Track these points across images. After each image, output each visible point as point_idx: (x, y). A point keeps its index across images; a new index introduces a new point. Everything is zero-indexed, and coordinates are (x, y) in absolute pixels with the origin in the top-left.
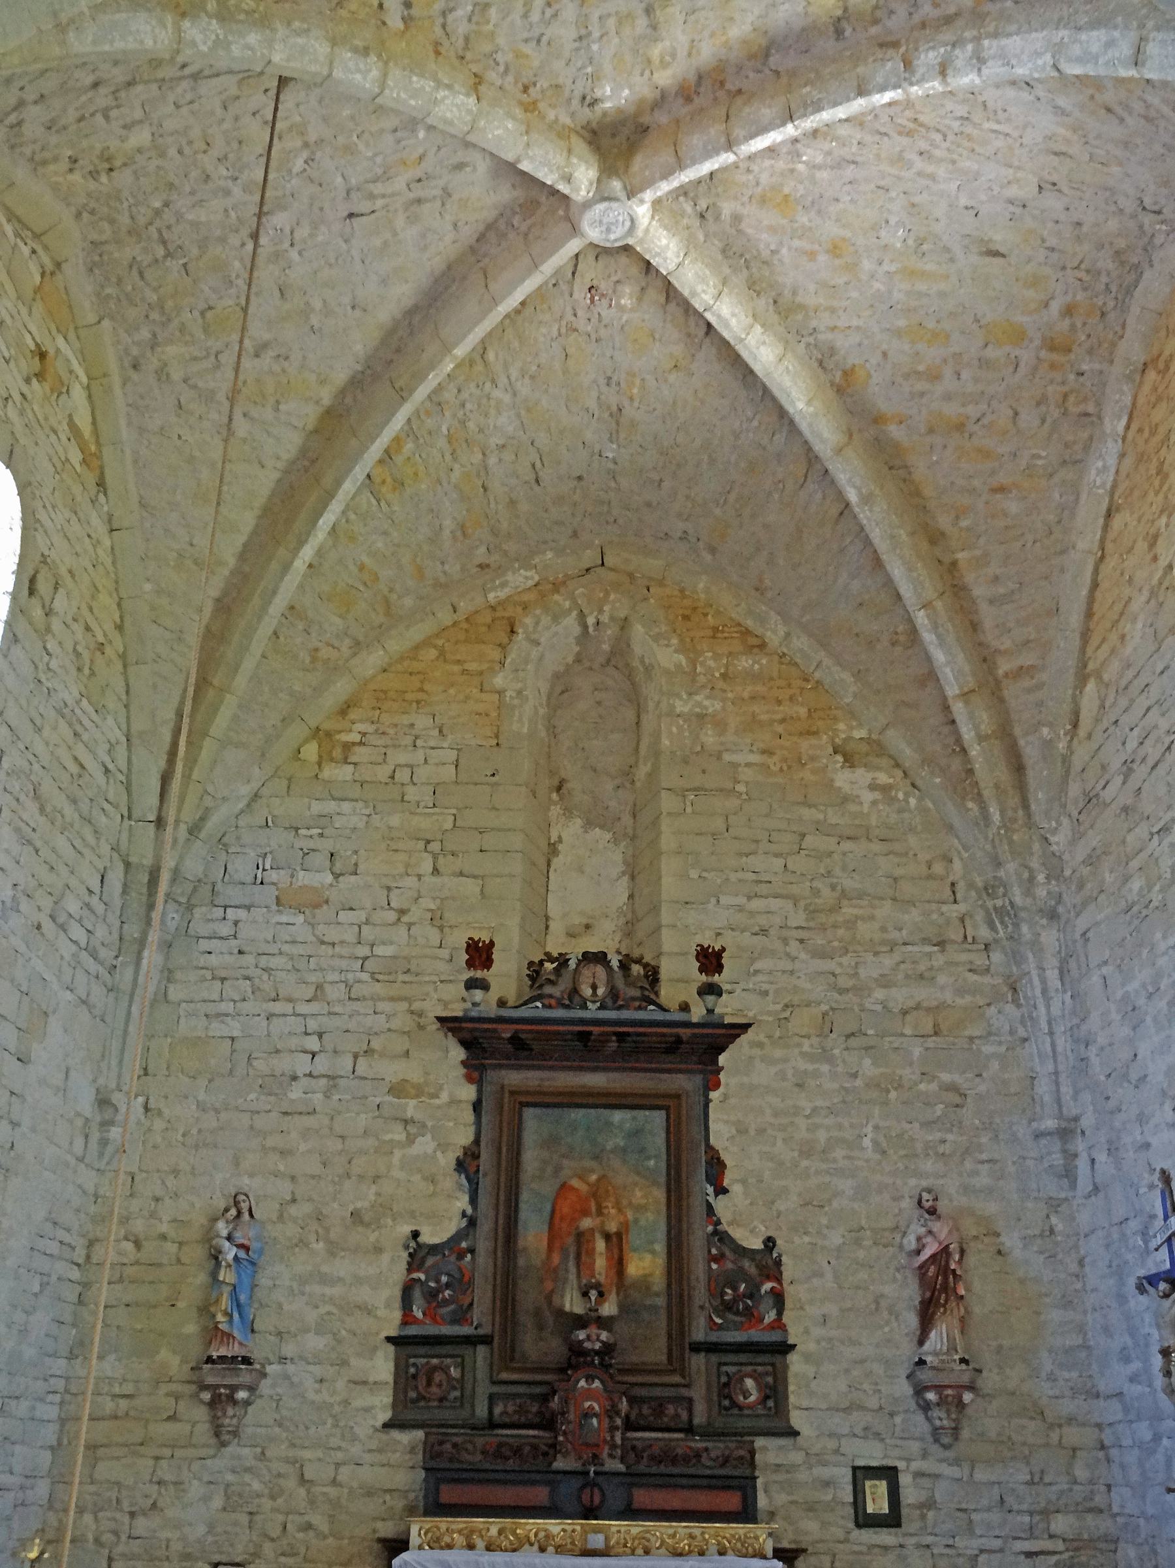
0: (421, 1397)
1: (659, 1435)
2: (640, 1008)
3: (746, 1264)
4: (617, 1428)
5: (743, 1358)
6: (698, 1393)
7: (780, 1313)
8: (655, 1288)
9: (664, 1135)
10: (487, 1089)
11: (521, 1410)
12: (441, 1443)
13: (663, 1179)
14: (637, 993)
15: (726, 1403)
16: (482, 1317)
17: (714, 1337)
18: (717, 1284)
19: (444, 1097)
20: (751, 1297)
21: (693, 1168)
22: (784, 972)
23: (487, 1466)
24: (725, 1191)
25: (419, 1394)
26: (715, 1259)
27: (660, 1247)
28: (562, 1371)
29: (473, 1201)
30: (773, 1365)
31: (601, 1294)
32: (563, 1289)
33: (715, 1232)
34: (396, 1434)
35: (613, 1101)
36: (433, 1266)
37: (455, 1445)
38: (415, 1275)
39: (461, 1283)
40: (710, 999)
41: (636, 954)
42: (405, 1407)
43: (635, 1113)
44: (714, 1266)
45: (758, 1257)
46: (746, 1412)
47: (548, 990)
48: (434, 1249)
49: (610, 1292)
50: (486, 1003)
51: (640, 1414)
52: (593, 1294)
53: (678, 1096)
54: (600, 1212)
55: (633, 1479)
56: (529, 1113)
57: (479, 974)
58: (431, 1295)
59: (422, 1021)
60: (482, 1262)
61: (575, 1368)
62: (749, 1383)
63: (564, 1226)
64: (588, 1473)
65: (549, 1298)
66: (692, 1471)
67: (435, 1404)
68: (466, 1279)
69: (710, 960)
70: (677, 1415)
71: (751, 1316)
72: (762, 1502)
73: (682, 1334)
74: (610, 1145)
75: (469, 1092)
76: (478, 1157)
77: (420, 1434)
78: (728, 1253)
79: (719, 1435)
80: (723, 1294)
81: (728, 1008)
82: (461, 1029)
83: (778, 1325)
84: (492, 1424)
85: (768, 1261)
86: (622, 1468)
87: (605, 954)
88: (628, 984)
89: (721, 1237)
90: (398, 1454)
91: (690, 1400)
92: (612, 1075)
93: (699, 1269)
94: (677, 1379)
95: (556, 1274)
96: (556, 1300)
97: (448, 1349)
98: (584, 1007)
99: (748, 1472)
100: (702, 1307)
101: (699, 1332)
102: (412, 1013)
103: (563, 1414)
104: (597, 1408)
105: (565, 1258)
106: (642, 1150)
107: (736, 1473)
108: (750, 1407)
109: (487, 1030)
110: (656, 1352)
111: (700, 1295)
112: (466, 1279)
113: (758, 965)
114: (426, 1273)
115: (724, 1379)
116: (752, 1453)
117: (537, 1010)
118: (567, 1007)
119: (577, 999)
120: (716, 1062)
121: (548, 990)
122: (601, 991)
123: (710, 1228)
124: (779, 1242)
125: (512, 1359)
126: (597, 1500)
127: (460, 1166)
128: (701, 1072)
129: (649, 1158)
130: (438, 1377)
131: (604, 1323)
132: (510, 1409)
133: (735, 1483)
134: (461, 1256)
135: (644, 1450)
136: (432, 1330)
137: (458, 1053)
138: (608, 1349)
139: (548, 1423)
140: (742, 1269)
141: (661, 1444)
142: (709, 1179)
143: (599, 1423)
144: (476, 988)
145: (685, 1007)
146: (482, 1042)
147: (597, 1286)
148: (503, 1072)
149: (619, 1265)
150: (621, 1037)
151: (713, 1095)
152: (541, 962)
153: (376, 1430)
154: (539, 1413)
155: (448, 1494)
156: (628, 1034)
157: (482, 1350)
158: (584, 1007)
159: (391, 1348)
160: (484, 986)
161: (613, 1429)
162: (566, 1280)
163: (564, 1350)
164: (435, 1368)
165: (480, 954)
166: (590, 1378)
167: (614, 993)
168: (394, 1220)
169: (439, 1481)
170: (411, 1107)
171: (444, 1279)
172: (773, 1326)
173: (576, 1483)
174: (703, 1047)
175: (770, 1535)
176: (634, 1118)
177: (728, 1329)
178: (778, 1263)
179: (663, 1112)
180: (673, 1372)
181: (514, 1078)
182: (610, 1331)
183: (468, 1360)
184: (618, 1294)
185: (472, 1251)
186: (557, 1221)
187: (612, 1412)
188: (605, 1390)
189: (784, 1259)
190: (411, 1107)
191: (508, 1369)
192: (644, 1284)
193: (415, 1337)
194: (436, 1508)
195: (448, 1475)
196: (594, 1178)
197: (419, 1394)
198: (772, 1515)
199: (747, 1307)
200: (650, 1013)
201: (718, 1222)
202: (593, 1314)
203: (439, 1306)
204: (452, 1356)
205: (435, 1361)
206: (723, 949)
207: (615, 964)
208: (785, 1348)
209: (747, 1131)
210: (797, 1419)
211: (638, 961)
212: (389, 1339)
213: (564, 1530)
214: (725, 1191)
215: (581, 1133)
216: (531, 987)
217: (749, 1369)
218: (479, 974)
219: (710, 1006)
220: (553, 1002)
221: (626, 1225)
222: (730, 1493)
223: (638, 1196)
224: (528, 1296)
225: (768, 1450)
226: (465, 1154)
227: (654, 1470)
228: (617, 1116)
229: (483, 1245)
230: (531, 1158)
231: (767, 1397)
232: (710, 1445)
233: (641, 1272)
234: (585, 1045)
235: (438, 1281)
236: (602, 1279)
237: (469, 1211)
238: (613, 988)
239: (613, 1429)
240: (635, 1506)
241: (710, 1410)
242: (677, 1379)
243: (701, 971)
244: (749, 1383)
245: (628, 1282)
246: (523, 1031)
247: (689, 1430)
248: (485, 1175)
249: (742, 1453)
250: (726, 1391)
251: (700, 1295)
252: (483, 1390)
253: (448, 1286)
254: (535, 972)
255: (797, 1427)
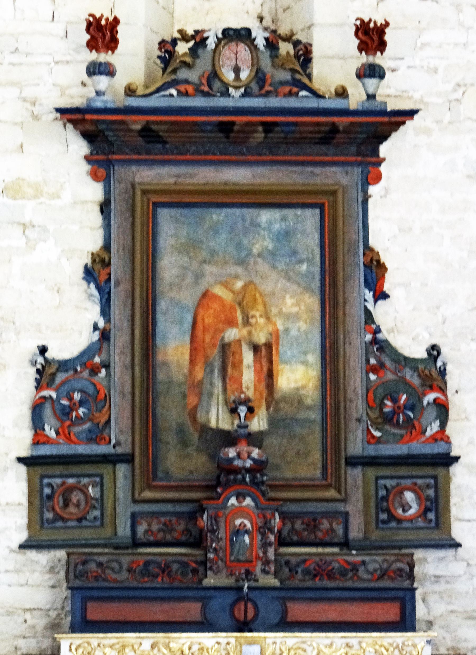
0: (58, 518)
1: (313, 550)
2: (290, 94)
3: (409, 374)
4: (270, 544)
5: (403, 471)
6: (355, 507)
7: (443, 425)
8: (309, 401)
9: (317, 236)
10: (116, 189)
11: (168, 528)
12: (84, 563)
13: (316, 284)
14: (286, 76)
15: (384, 516)
16: (120, 434)
17: (371, 451)
18: (374, 399)
19: (67, 197)
20: (412, 408)
21: (348, 272)
22: (456, 45)
23: (135, 584)
24: (385, 296)
25: (56, 514)
26: (374, 369)
27: (314, 358)
28: (210, 488)
29: (105, 311)
30: (435, 478)
31: (251, 410)
32: (209, 405)
33: (375, 341)
34: (32, 554)
35: (260, 199)
36: (63, 383)
37: (100, 564)
38: (45, 393)
39: (97, 400)
40: (371, 83)
41: (283, 30)
42: (42, 526)
43: (289, 212)
44: (373, 377)
45: (421, 366)
46: (405, 525)
47: (183, 74)
48: (64, 365)
49: (260, 407)
50: (111, 91)
51: (293, 529)
52: (243, 410)
53: (334, 193)
54: (247, 322)
55: (287, 593)
56: (164, 215)
57: (103, 57)
58: (64, 414)
59: (36, 110)
60: (119, 378)
61: (226, 486)
62: (409, 496)
63: (208, 338)
64: (241, 588)
65: (193, 415)
66: (349, 584)
67: (74, 523)
68: (102, 395)
69: (371, 37)
70: (332, 530)
71: (412, 428)
72: (421, 611)
73: (337, 450)
74: (256, 249)
75: (95, 192)
76: (109, 264)
77: (61, 554)
78: (388, 363)
79: (377, 548)
80: (382, 405)
81: (391, 93)
82: (83, 121)
83: (442, 436)
84: (136, 543)
85: (431, 370)
86: (275, 582)
87: (248, 31)
88: (274, 66)
89: (381, 346)
90: (37, 575)
91: (346, 514)
92: (260, 170)
93: (356, 380)
94: (332, 493)
95: (198, 388)
96: (201, 417)
97: (87, 469)
98: (226, 94)
99: (406, 584)
100: (359, 420)
101: (356, 445)
102: (24, 100)
103: (213, 531)
104: (249, 525)
105: (209, 367)
106: (294, 253)
107: (393, 585)
108: (410, 520)
109: (113, 122)
110: (309, 467)
111: (357, 406)
112: (102, 395)
113: (425, 38)
114: (57, 390)
115: (382, 493)
116: (412, 566)
117: (172, 98)
118: (206, 94)
119: (217, 85)
120: (376, 152)
121: (183, 74)
122: (244, 75)
123: (369, 337)
124: (444, 350)
125: (155, 477)
126: (251, 614)
127: (89, 274)
128: (359, 164)
129: (301, 262)
130: (76, 497)
131: (255, 439)
132: (155, 527)
133: (393, 594)
134: (94, 371)
135: (298, 565)
136: (65, 449)
137: (79, 147)
138: (259, 466)
139: (197, 541)
140: (403, 379)
141: (317, 559)
142: (367, 285)
143: (251, 540)
144: (101, 73)
145: (342, 93)
146: (104, 133)
147: (246, 401)
148: (134, 168)
149: (269, 377)
150: (268, 127)
151: (372, 190)
152: (174, 42)
153: (12, 551)
154: (187, 530)
155: (95, 612)
156: (275, 124)
157: (122, 470)
158: (226, 94)
159: (23, 469)
160: (108, 70)
161: (266, 545)
162: (211, 395)
163: (212, 468)
164: (71, 489)
165: (103, 34)
166: (240, 496)
167: (259, 77)
168: (18, 333)
169: (85, 601)
170: (29, 210)
171: (77, 396)
172: (434, 439)
173: (230, 597)
174: (362, 135)
175: (429, 642)
176: (284, 219)
177: (386, 442)
178: (443, 373)
179: (317, 211)
180: (328, 486)
181: (147, 175)
182: (260, 447)
183: (107, 479)
184: (268, 408)
185: (107, 366)
186: (199, 332)
187: (264, 529)
188: (257, 507)
189: (448, 368)
190: (29, 210)
191: (150, 487)
192: (296, 400)
193: (51, 457)
194: (84, 625)
195: (96, 594)
196: (239, 284)
197: (56, 514)
198: (430, 624)
199: (408, 419)
200: (303, 100)
201: (378, 330)
202: (242, 431)
203: (73, 424)
204: (89, 476)
205: (71, 481)
206: (387, 24)
207: (260, 42)
208: (448, 460)
209: (410, 229)
210: (458, 531)
211: (288, 39)
212: (20, 460)
213: (218, 643)
214: (385, 296)
215: (223, 236)
216: (164, 70)
217: (408, 482)
218: (103, 57)
219: (371, 91)
220: (190, 89)
221: (276, 334)
222: (397, 609)
223: (289, 304)
224: (171, 414)
225: (429, 563)
226: (94, 261)
227: (309, 584)
228: (265, 216)
229: (119, 361)
230: (169, 265)
231: (427, 510)
232: (367, 558)
233: (293, 385)
234: (227, 136)
235: (71, 399)
236: (250, 393)
237: (101, 324)
238: (258, 70)
239: (266, 545)
240: (290, 618)
241: (366, 524)
242: (332, 493)
243: (360, 49)
244: (409, 496)
245: (277, 396)
246: (155, 123)
247: (345, 544)
248: (118, 283)
249: (400, 565)
250: (384, 507)
251: (357, 406)
252: (124, 510)
253: (81, 403)
254: (167, 49)
255: (459, 540)
